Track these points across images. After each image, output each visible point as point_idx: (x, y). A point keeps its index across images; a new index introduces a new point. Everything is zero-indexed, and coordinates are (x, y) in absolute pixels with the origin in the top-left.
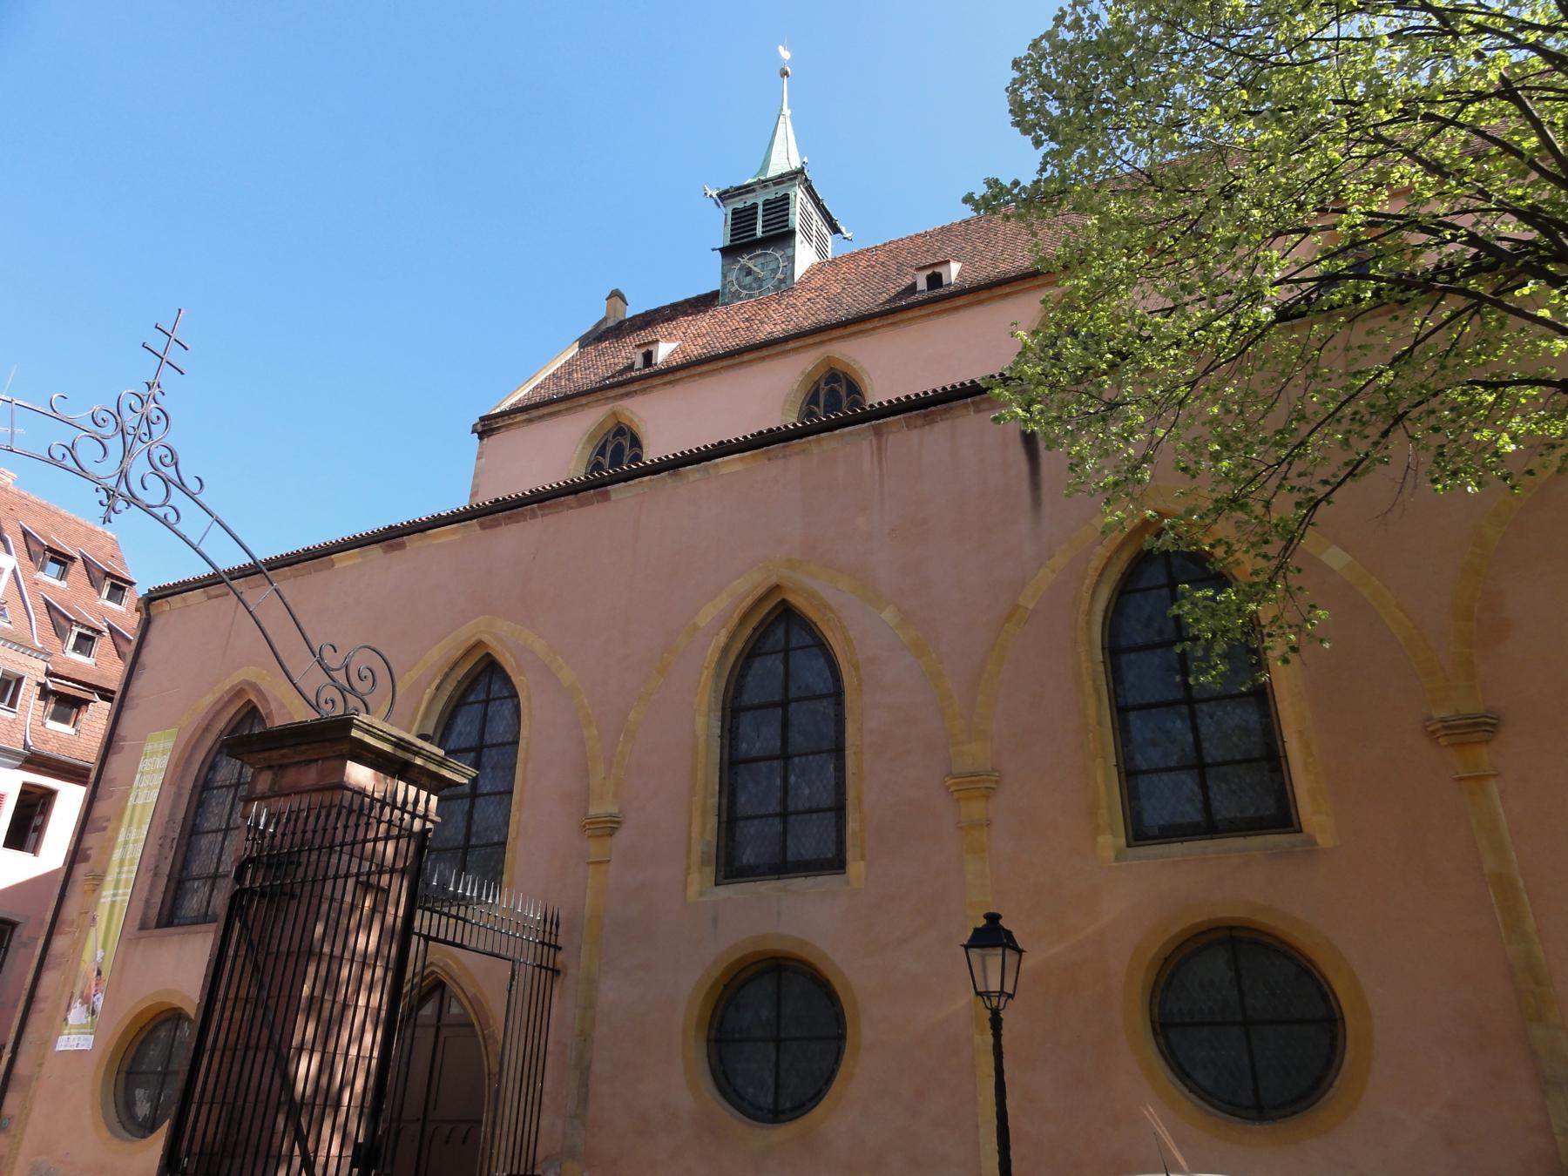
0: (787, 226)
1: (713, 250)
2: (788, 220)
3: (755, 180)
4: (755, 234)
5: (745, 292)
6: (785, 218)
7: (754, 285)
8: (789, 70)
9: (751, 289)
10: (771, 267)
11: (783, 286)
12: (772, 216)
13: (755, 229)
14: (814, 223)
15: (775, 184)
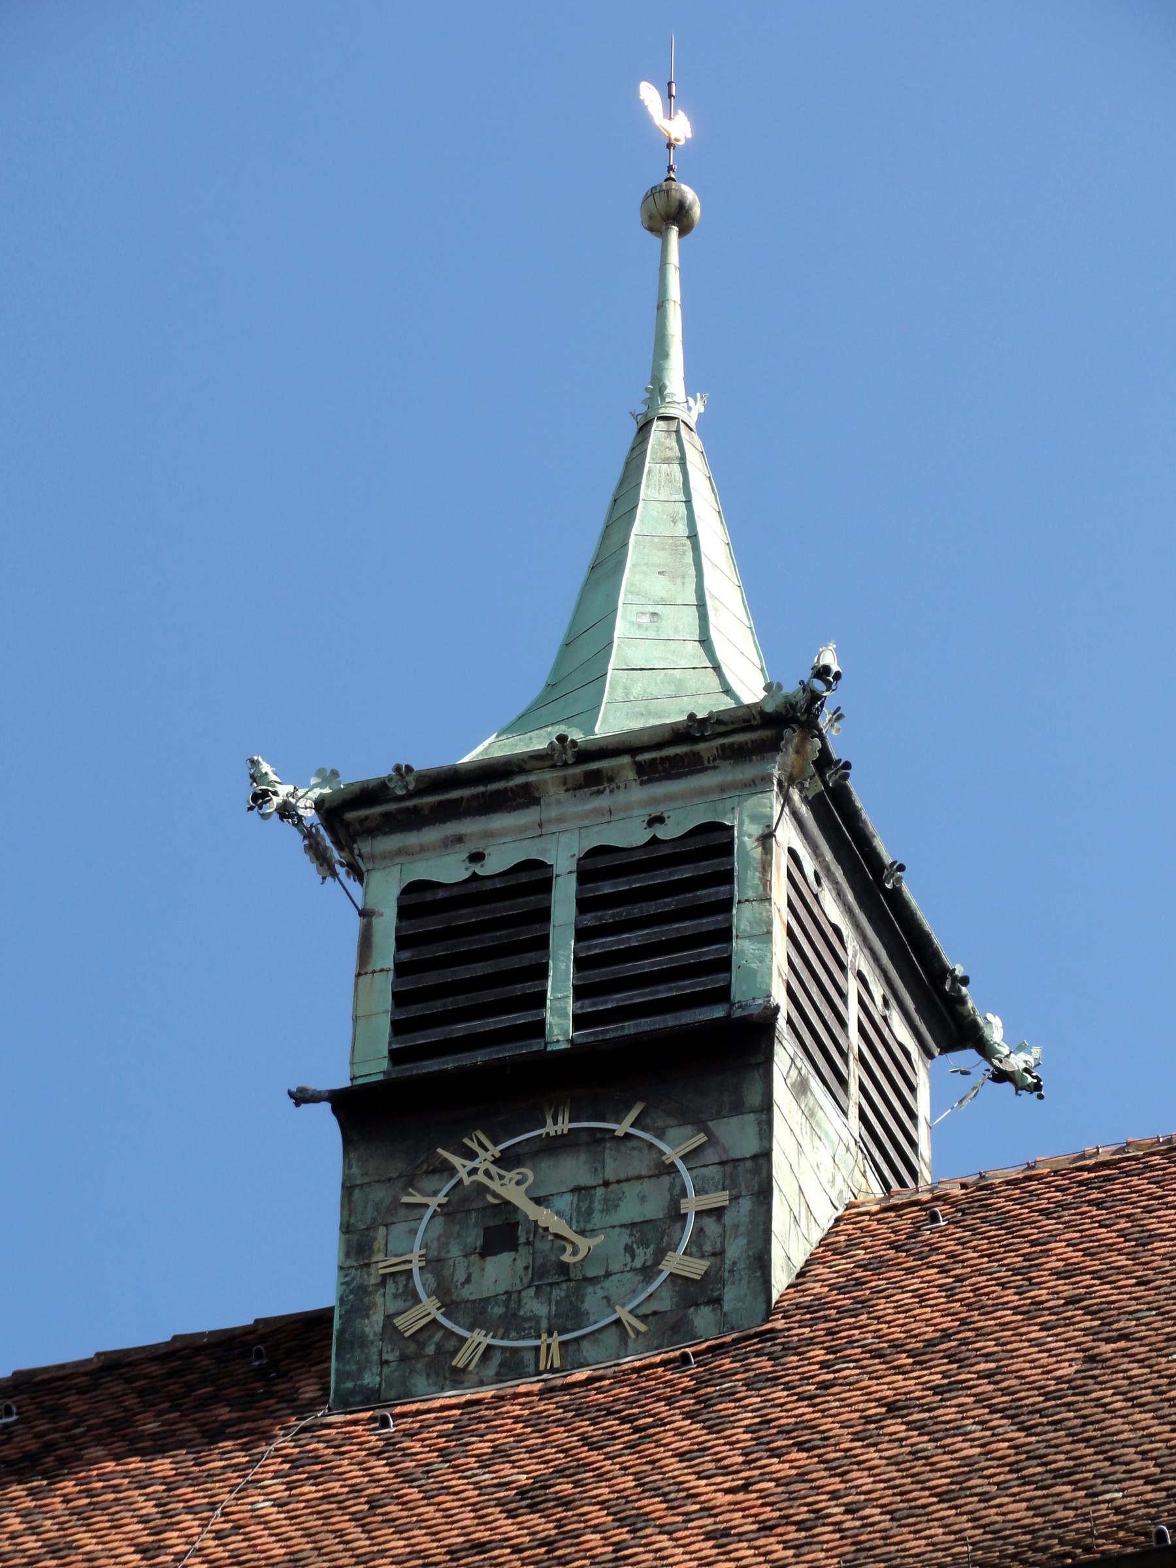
0: (723, 994)
1: (301, 1097)
2: (724, 964)
3: (539, 741)
4: (538, 1029)
5: (479, 1338)
6: (709, 952)
7: (535, 1307)
8: (690, 195)
9: (512, 1322)
10: (630, 1210)
11: (703, 1319)
12: (633, 939)
13: (539, 1000)
14: (852, 987)
15: (649, 773)
